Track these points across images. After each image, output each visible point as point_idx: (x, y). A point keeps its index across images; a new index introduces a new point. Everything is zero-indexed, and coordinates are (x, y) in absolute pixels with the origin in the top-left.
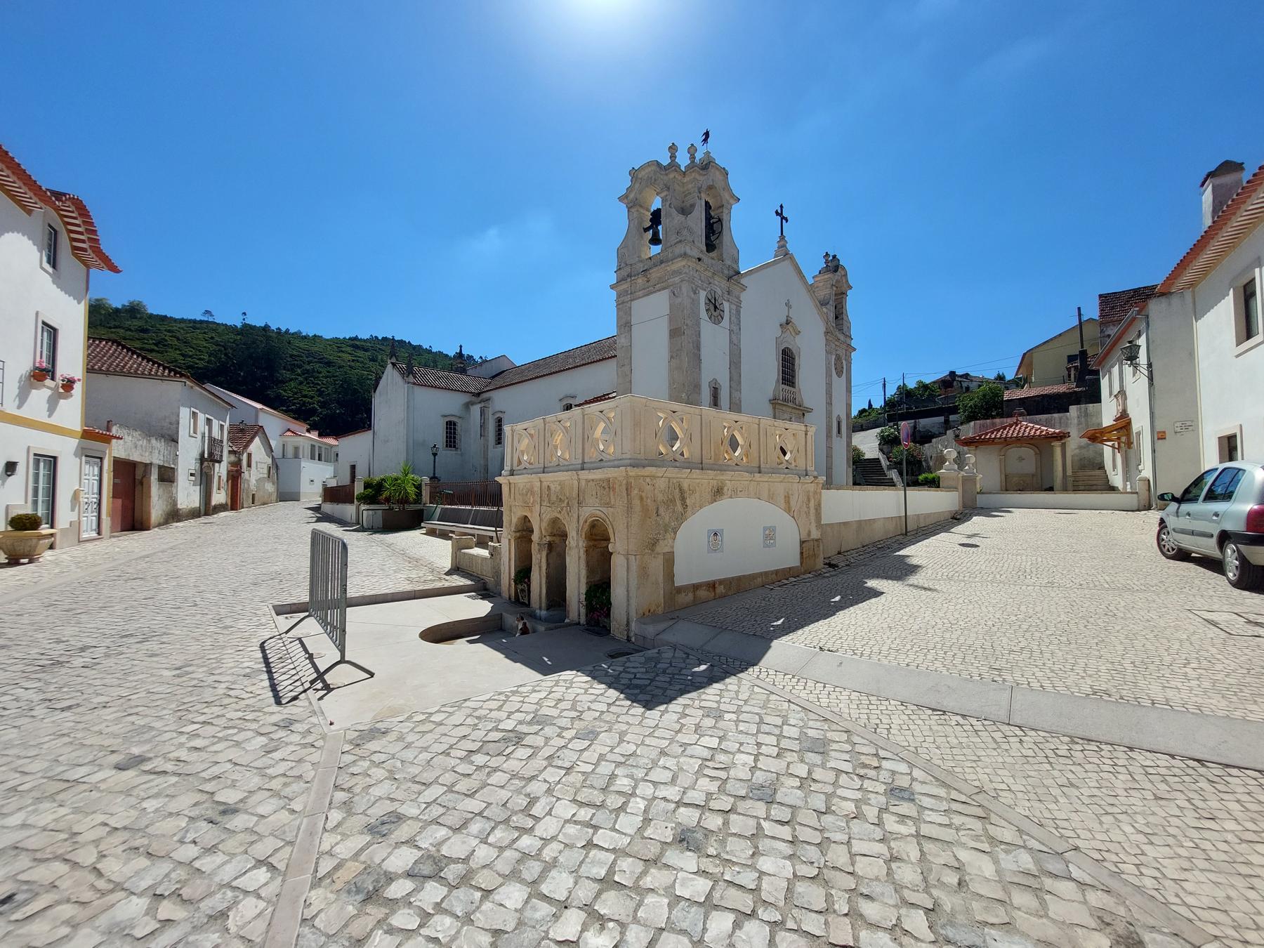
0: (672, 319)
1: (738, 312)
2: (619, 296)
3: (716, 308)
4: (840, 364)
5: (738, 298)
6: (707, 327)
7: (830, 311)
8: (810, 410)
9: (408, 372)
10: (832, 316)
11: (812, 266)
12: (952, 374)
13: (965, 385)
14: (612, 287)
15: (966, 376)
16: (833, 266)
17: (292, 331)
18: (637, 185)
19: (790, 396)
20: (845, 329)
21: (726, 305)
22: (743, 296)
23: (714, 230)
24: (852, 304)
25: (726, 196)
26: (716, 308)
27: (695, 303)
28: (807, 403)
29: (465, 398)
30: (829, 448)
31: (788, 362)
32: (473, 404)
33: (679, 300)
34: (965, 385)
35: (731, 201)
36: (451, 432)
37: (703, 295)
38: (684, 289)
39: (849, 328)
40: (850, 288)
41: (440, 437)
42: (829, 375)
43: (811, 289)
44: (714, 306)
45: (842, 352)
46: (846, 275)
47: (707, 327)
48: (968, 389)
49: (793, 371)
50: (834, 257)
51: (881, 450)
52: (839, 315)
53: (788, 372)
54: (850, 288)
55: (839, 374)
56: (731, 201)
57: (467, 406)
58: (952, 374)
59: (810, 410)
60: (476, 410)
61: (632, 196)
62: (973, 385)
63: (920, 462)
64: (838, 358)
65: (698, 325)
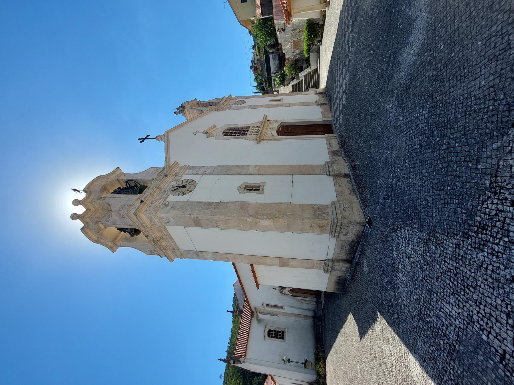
0: (186, 225)
1: (192, 168)
2: (177, 257)
3: (183, 187)
4: (238, 102)
5: (182, 167)
6: (195, 196)
7: (205, 109)
8: (265, 117)
9: (237, 360)
10: (209, 108)
11: (181, 119)
12: (251, 67)
13: (256, 62)
14: (171, 260)
15: (252, 61)
16: (181, 109)
17: (229, 341)
18: (103, 241)
19: (255, 130)
20: (218, 101)
21: (185, 178)
22: (182, 164)
23: (133, 187)
24: (204, 98)
25: (114, 177)
26: (183, 187)
27: (176, 206)
28: (260, 119)
29: (254, 321)
30: (290, 105)
31: (232, 132)
32: (257, 317)
33: (171, 219)
34: (256, 62)
35: (118, 173)
36: (276, 334)
37: (172, 198)
38: (163, 215)
39: (218, 99)
40: (196, 99)
41: (275, 342)
42: (244, 108)
43: (189, 121)
44: (182, 188)
45: (231, 102)
46: (188, 102)
47: (195, 196)
48: (257, 60)
49: (239, 128)
50: (178, 109)
51: (287, 85)
52: (210, 104)
53: (239, 132)
54: (196, 99)
55: (244, 102)
56: (118, 173)
57: (259, 321)
58: (251, 67)
59: (265, 117)
60: (261, 316)
61: (110, 244)
62: (256, 58)
63: (296, 60)
64: (234, 103)
65: (193, 203)
